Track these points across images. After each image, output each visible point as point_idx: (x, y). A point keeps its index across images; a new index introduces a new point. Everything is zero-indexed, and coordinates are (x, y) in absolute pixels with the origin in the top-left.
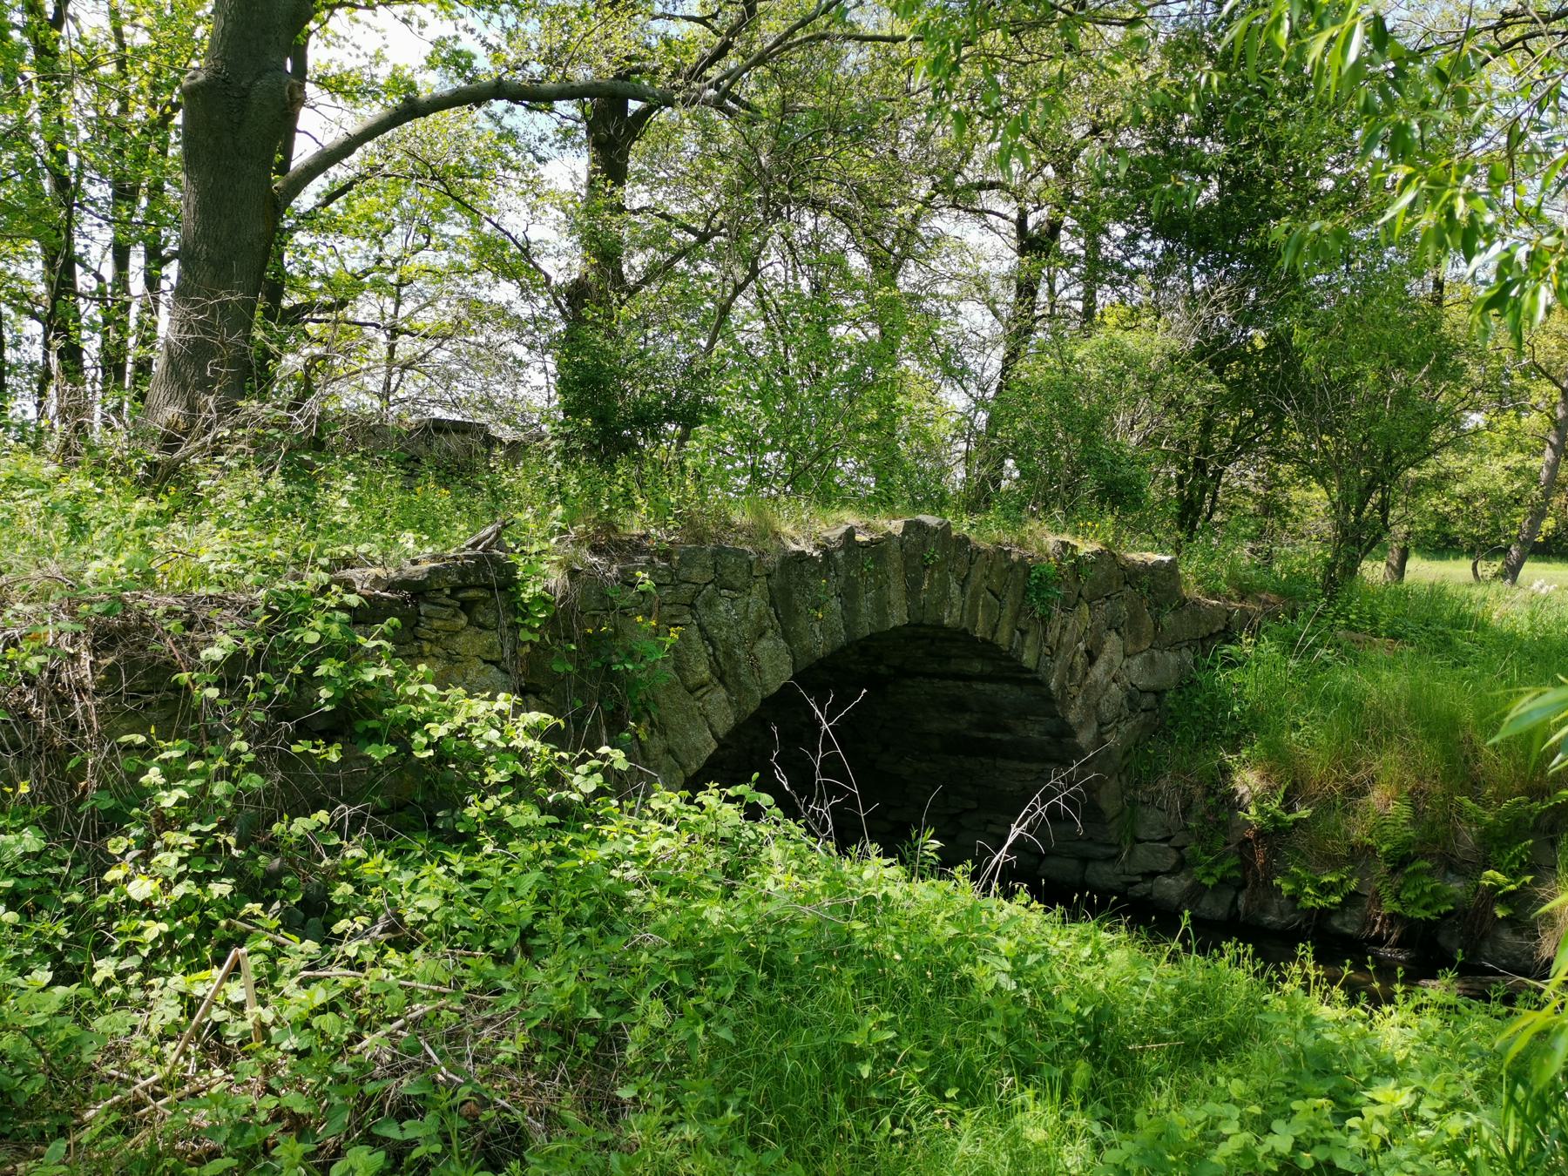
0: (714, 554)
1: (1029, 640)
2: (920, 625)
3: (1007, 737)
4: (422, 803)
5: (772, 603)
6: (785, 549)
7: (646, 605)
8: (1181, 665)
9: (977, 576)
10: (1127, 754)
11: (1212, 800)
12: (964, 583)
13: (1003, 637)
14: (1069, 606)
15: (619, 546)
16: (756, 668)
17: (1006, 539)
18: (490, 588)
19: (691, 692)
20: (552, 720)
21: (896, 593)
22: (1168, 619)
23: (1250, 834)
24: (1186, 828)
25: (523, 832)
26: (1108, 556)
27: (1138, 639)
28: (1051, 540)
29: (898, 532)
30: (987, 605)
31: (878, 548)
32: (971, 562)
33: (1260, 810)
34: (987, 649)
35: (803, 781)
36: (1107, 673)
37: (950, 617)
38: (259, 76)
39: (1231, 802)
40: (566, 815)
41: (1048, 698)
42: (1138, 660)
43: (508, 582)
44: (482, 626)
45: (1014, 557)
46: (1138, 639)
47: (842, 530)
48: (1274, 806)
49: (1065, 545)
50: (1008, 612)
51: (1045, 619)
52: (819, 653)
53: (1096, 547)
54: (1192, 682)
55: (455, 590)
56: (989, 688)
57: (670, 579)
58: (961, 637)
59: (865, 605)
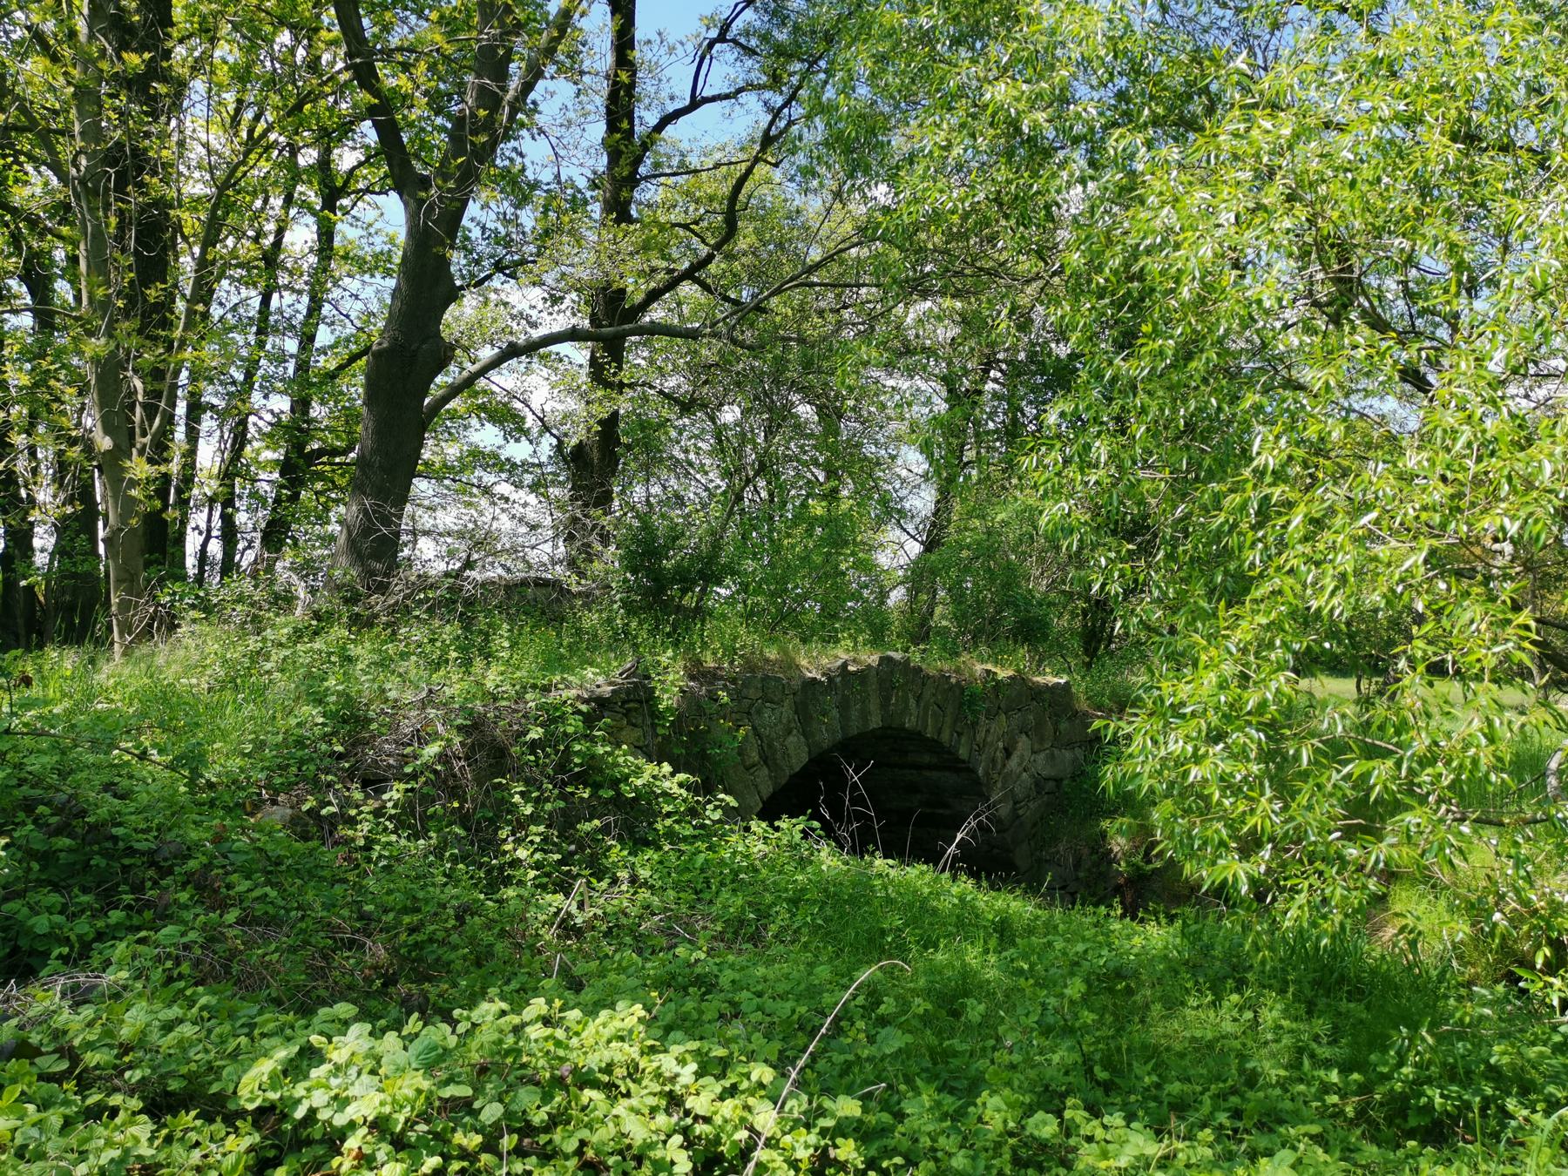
0: (763, 680)
1: (963, 740)
2: (890, 728)
3: (948, 812)
4: (635, 819)
5: (796, 712)
6: (802, 676)
7: (723, 711)
8: (1075, 759)
9: (927, 694)
10: (1035, 825)
11: (1095, 857)
12: (918, 699)
13: (945, 737)
14: (991, 715)
15: (704, 675)
16: (786, 755)
17: (946, 667)
18: (640, 702)
19: (747, 769)
20: (692, 779)
21: (874, 705)
22: (1064, 726)
23: (1121, 881)
24: (1077, 879)
25: (685, 839)
26: (1019, 680)
27: (1042, 740)
28: (979, 668)
29: (875, 665)
30: (934, 714)
31: (862, 676)
32: (924, 684)
33: (1128, 863)
34: (935, 746)
35: (837, 814)
36: (1020, 765)
37: (910, 723)
38: (424, 342)
39: (1107, 858)
40: (705, 833)
41: (977, 782)
42: (1042, 755)
43: (650, 698)
44: (635, 725)
45: (953, 681)
46: (1042, 740)
47: (840, 662)
48: (1138, 859)
49: (988, 672)
50: (948, 720)
51: (975, 724)
52: (825, 746)
53: (1011, 673)
54: (1083, 772)
55: (624, 703)
56: (935, 775)
57: (737, 696)
58: (916, 736)
59: (854, 714)
